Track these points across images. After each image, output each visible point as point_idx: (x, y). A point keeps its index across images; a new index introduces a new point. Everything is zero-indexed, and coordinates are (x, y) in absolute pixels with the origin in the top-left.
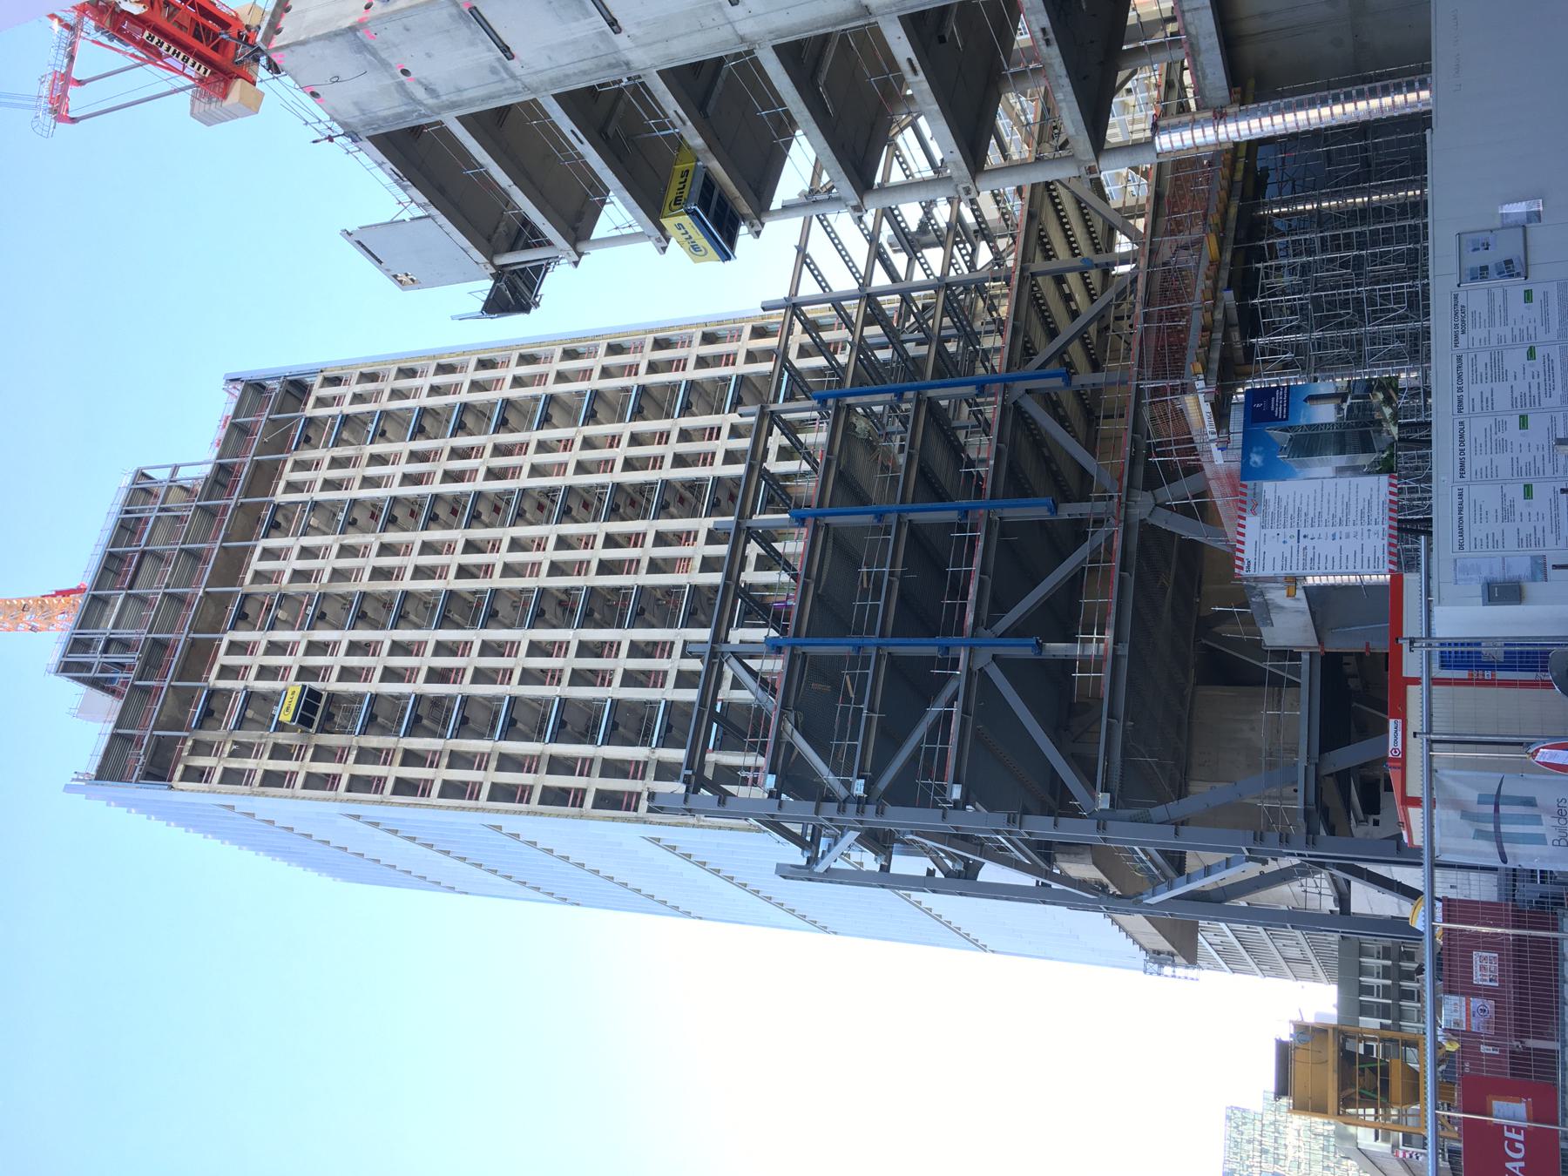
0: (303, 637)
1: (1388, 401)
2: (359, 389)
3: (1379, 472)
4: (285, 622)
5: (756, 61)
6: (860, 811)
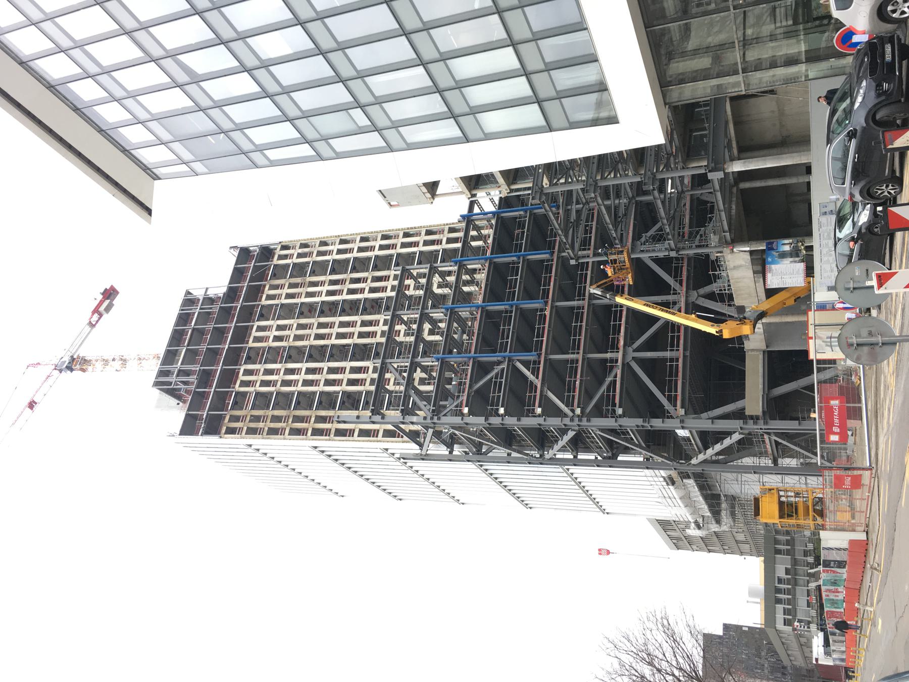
0: (282, 366)
1: (803, 245)
2: (300, 251)
4: (271, 360)
6: (580, 420)
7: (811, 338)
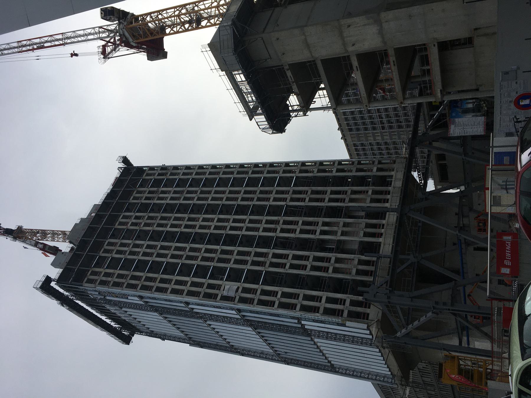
0: (132, 242)
3: (482, 116)
5: (315, 64)
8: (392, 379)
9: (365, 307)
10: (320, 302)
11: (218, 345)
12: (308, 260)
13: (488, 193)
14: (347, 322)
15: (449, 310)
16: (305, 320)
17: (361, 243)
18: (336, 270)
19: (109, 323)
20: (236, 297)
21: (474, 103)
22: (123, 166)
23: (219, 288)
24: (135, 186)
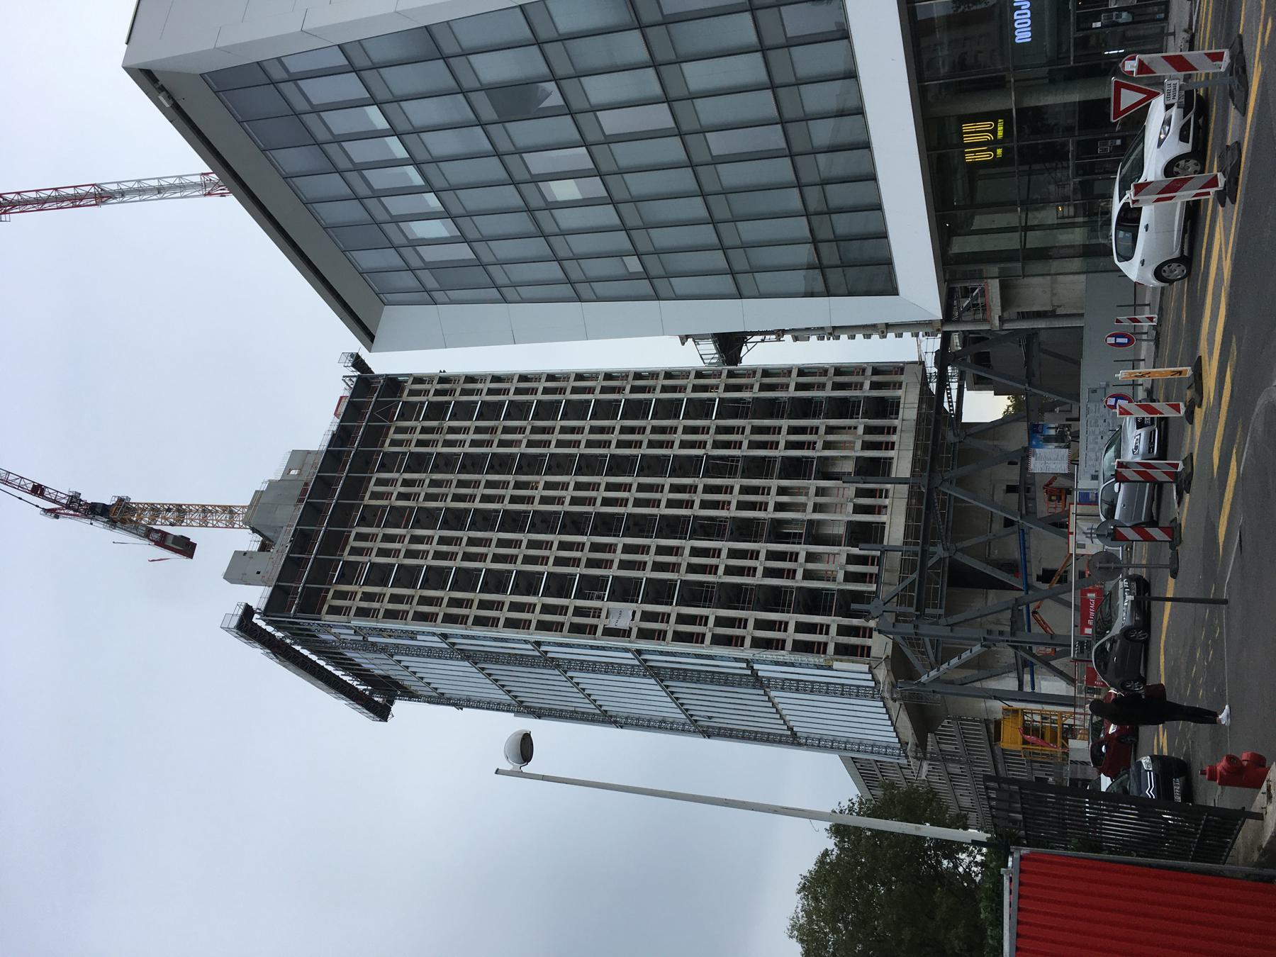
1: (1069, 430)
2: (439, 387)
7: (1072, 533)
8: (900, 750)
9: (864, 636)
10: (785, 630)
11: (576, 712)
12: (757, 558)
13: (1072, 538)
14: (835, 663)
15: (1007, 641)
16: (758, 662)
17: (849, 523)
18: (808, 575)
19: (351, 682)
20: (631, 629)
21: (1057, 428)
22: (352, 374)
23: (597, 614)
24: (388, 415)
